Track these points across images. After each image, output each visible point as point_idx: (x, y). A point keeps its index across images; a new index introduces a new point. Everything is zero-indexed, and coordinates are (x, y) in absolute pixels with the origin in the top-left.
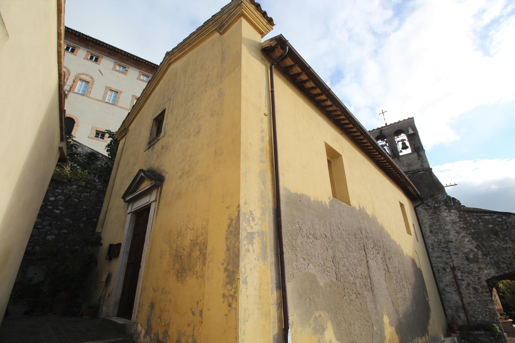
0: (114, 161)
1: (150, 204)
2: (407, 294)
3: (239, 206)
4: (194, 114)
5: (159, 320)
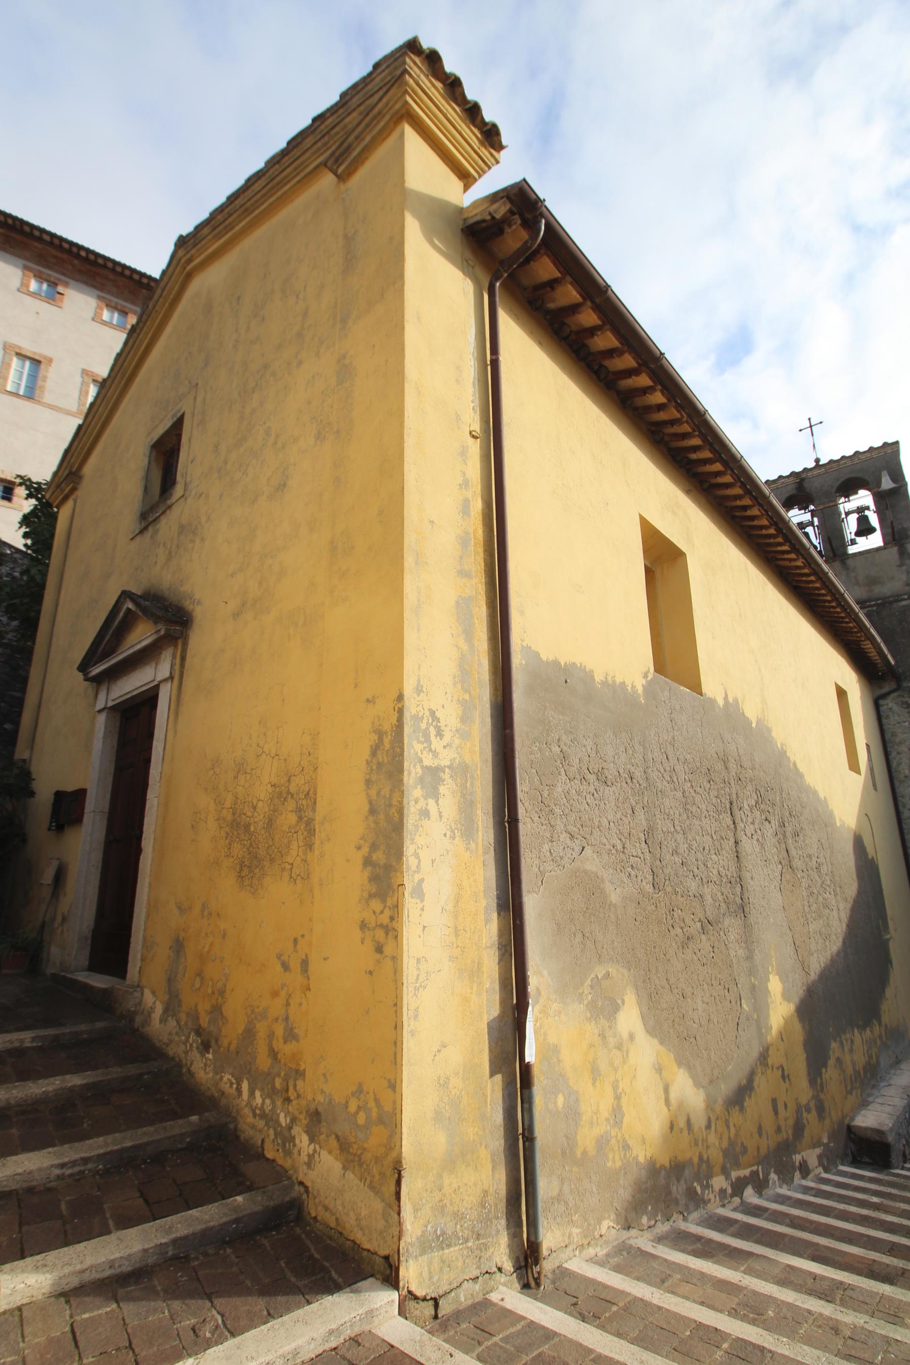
0: (48, 565)
1: (157, 687)
2: (835, 923)
3: (400, 698)
4: (268, 433)
5: (198, 980)
